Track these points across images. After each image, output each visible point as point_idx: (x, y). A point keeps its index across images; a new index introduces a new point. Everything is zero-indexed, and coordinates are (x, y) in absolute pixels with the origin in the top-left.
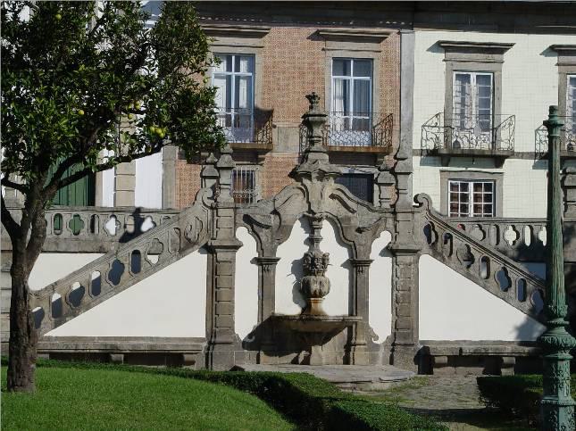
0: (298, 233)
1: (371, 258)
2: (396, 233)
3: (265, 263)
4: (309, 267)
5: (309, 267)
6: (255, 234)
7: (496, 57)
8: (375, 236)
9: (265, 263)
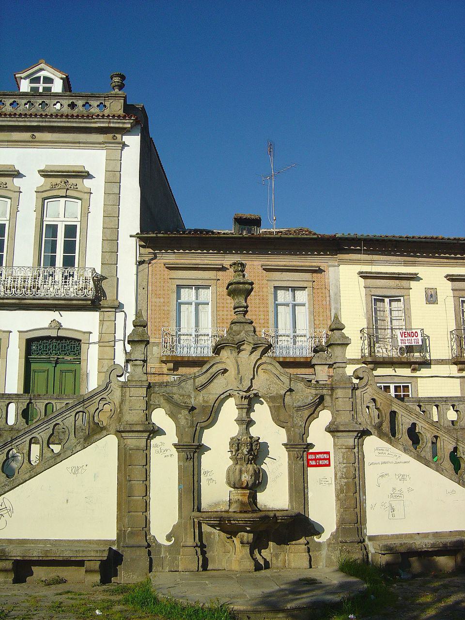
0: (230, 411)
1: (309, 441)
2: (335, 413)
3: (192, 450)
4: (251, 452)
5: (251, 452)
6: (172, 415)
7: (404, 283)
8: (313, 415)
9: (192, 450)
